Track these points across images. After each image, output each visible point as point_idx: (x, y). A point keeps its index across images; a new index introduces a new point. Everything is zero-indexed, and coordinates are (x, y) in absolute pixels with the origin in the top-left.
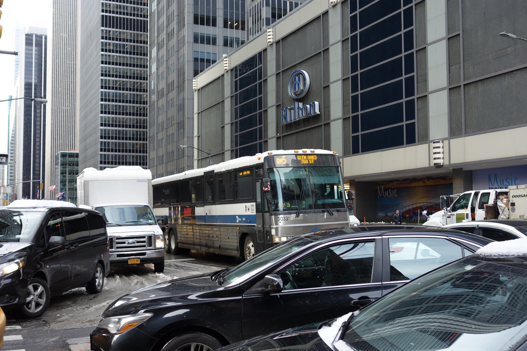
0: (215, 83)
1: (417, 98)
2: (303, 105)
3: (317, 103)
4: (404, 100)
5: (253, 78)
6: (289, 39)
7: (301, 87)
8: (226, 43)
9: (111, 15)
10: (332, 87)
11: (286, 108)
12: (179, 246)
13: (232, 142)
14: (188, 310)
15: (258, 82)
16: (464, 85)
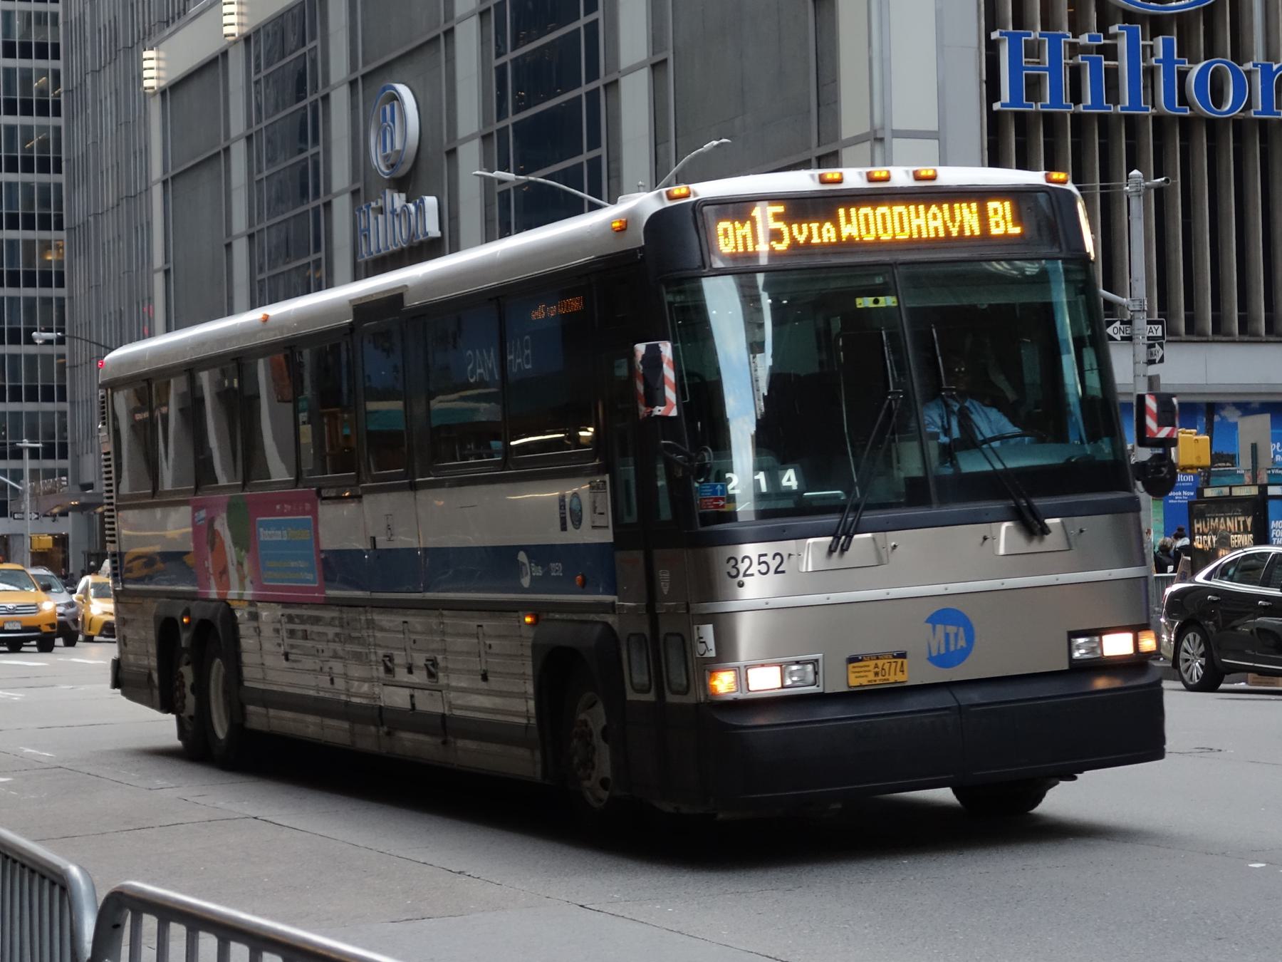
3: (431, 202)
7: (398, 146)
14: (221, 734)
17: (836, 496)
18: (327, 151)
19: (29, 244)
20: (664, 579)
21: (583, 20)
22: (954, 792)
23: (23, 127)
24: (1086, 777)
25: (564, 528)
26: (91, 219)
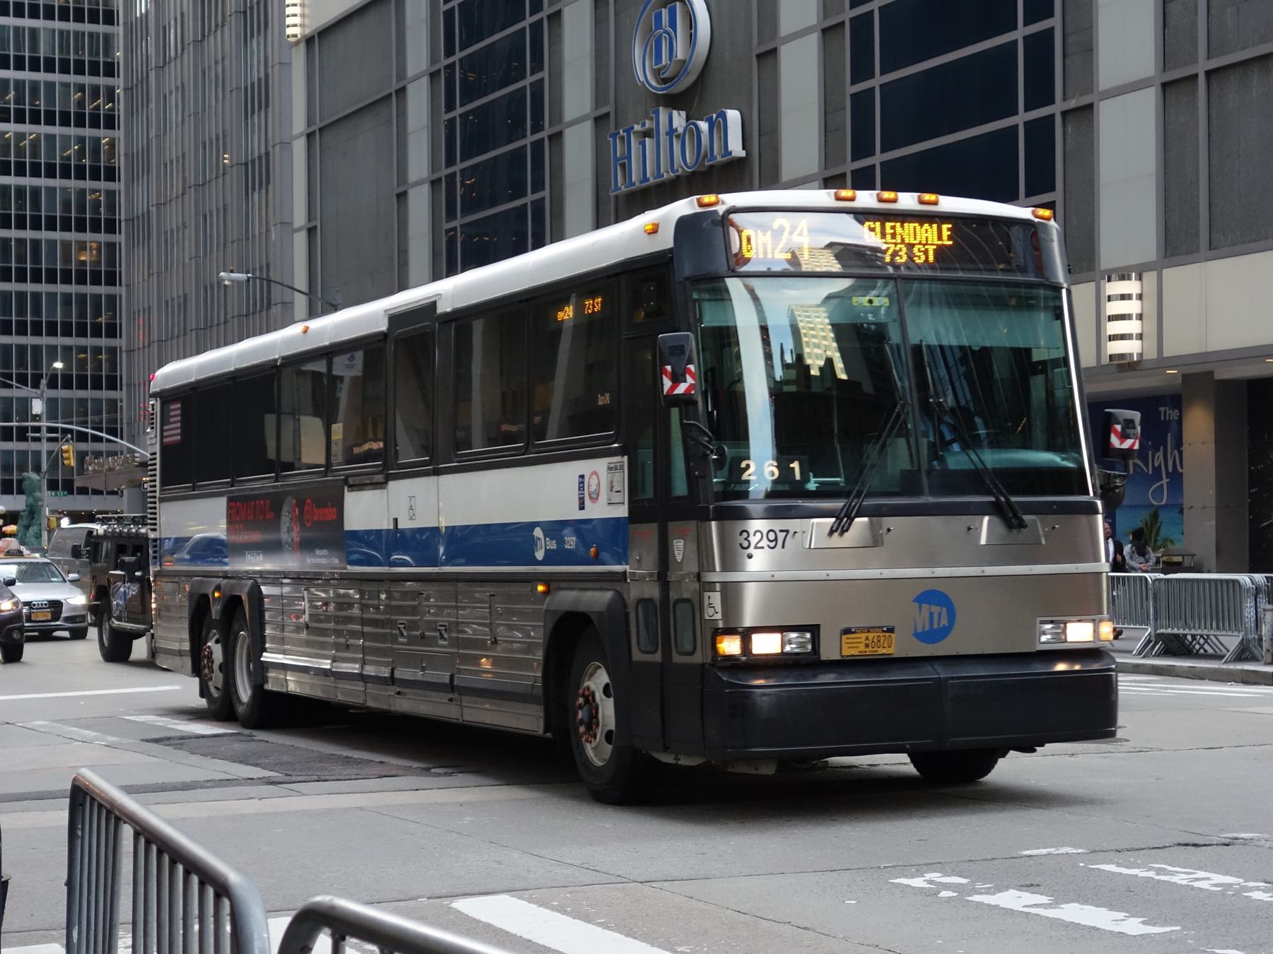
1: (1064, 114)
2: (688, 119)
3: (733, 116)
4: (1021, 118)
7: (680, 54)
10: (787, 55)
11: (628, 131)
12: (269, 687)
15: (530, 20)
16: (1209, 74)
17: (836, 483)
18: (557, 76)
19: (66, 245)
20: (679, 548)
21: (529, 79)
22: (914, 761)
23: (62, 136)
24: (1047, 745)
25: (582, 507)
26: (153, 210)
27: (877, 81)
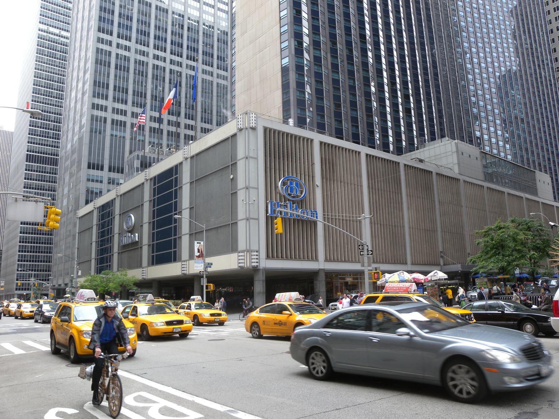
0: (89, 215)
3: (137, 234)
5: (169, 185)
6: (127, 195)
8: (111, 182)
9: (34, 154)
13: (149, 237)
15: (174, 189)
18: (114, 227)
27: (173, 225)
